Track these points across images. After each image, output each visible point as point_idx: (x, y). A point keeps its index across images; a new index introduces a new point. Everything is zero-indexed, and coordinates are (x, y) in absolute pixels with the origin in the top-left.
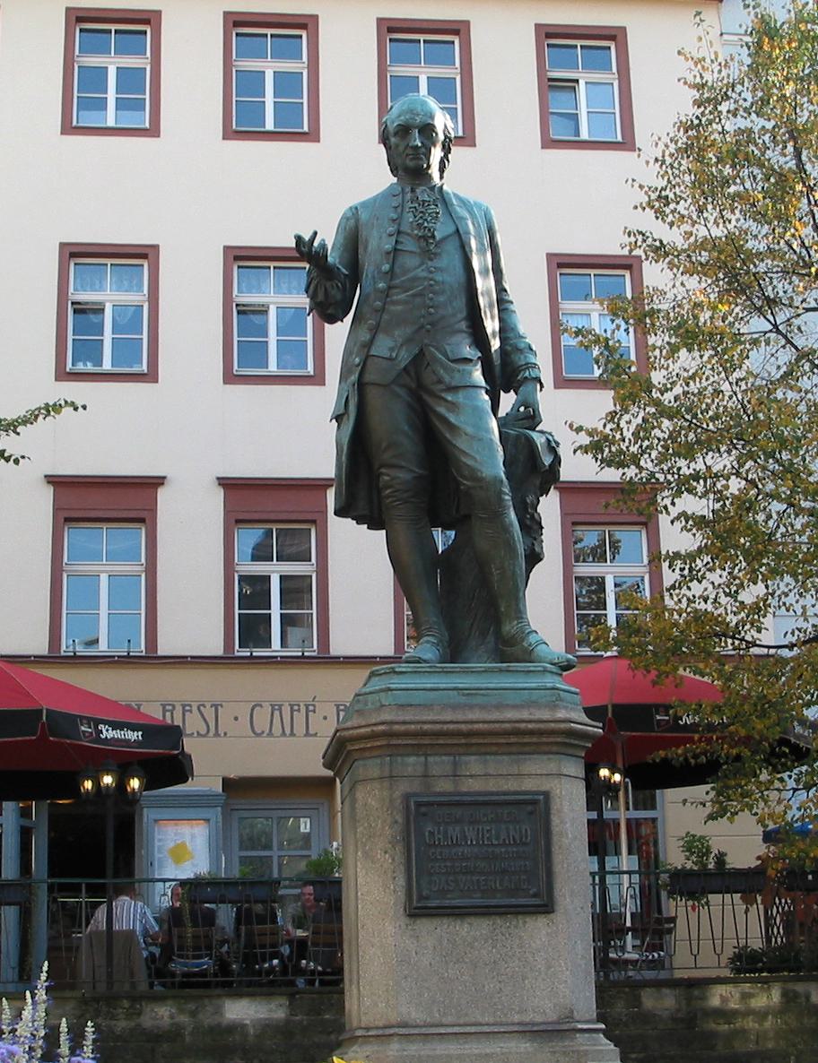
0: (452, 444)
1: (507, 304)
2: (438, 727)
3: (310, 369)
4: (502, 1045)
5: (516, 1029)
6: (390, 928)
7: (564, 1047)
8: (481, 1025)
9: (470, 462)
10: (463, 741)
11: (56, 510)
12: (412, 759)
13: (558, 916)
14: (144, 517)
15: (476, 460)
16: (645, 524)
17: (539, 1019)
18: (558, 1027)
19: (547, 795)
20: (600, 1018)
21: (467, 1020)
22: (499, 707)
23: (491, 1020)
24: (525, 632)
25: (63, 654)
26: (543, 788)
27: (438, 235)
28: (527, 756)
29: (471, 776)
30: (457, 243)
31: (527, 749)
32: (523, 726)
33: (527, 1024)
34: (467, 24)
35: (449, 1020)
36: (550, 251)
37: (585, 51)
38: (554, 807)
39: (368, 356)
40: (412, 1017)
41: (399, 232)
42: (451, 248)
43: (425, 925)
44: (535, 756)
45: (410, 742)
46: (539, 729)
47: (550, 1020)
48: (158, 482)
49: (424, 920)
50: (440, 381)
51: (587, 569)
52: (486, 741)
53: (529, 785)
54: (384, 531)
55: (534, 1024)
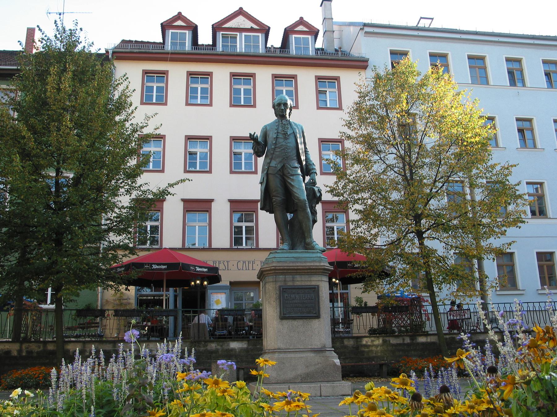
2: (288, 267)
3: (254, 170)
6: (275, 322)
9: (297, 195)
12: (281, 276)
13: (321, 319)
14: (208, 210)
17: (316, 347)
19: (318, 286)
20: (333, 347)
22: (305, 262)
23: (303, 348)
24: (312, 242)
27: (288, 133)
30: (294, 136)
31: (313, 273)
32: (312, 267)
35: (291, 347)
38: (320, 289)
43: (285, 322)
49: (285, 320)
50: (289, 173)
51: (329, 224)
53: (313, 283)
55: (315, 349)
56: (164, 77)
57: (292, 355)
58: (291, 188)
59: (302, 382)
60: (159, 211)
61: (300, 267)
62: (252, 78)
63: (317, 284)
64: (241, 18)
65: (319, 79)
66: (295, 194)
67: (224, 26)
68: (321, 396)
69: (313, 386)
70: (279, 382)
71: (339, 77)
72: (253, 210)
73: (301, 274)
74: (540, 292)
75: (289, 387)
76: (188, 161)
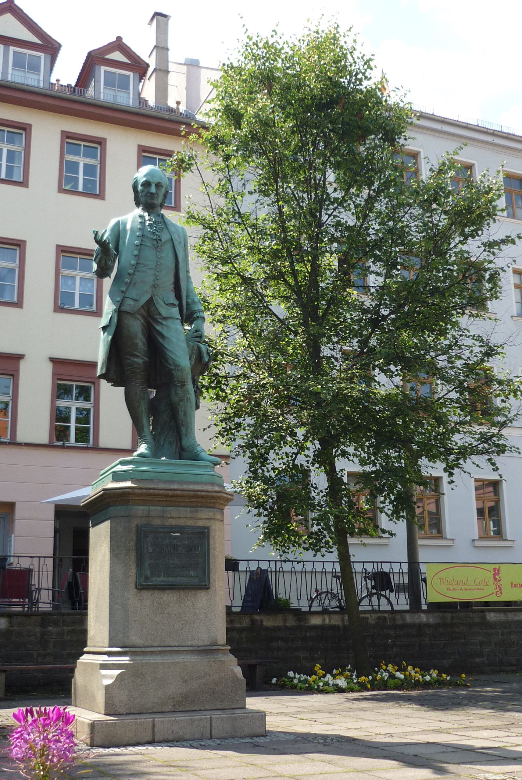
0: (164, 346)
2: (157, 491)
3: (94, 308)
4: (183, 657)
7: (214, 658)
8: (172, 646)
9: (173, 356)
10: (168, 499)
11: (54, 374)
12: (141, 507)
15: (176, 355)
16: (13, 375)
17: (201, 643)
18: (210, 648)
19: (208, 528)
21: (165, 644)
22: (187, 483)
23: (177, 644)
24: (195, 445)
27: (163, 240)
28: (200, 509)
29: (171, 518)
30: (171, 245)
32: (199, 493)
33: (195, 646)
34: (30, 126)
35: (155, 644)
36: (59, 244)
37: (85, 148)
38: (212, 534)
39: (124, 297)
40: (138, 642)
41: (143, 236)
42: (168, 247)
43: (146, 594)
44: (203, 509)
45: (142, 498)
47: (206, 644)
49: (145, 591)
50: (160, 314)
51: (62, 403)
52: (180, 500)
53: (200, 523)
54: (123, 389)
55: (199, 646)
57: (158, 659)
58: (160, 340)
59: (174, 712)
61: (178, 492)
62: (24, 132)
63: (206, 525)
64: (8, 17)
65: (68, 137)
66: (167, 352)
67: (108, 57)
68: (211, 738)
70: (132, 711)
71: (105, 140)
74: (477, 543)
75: (154, 720)
76: (16, 284)
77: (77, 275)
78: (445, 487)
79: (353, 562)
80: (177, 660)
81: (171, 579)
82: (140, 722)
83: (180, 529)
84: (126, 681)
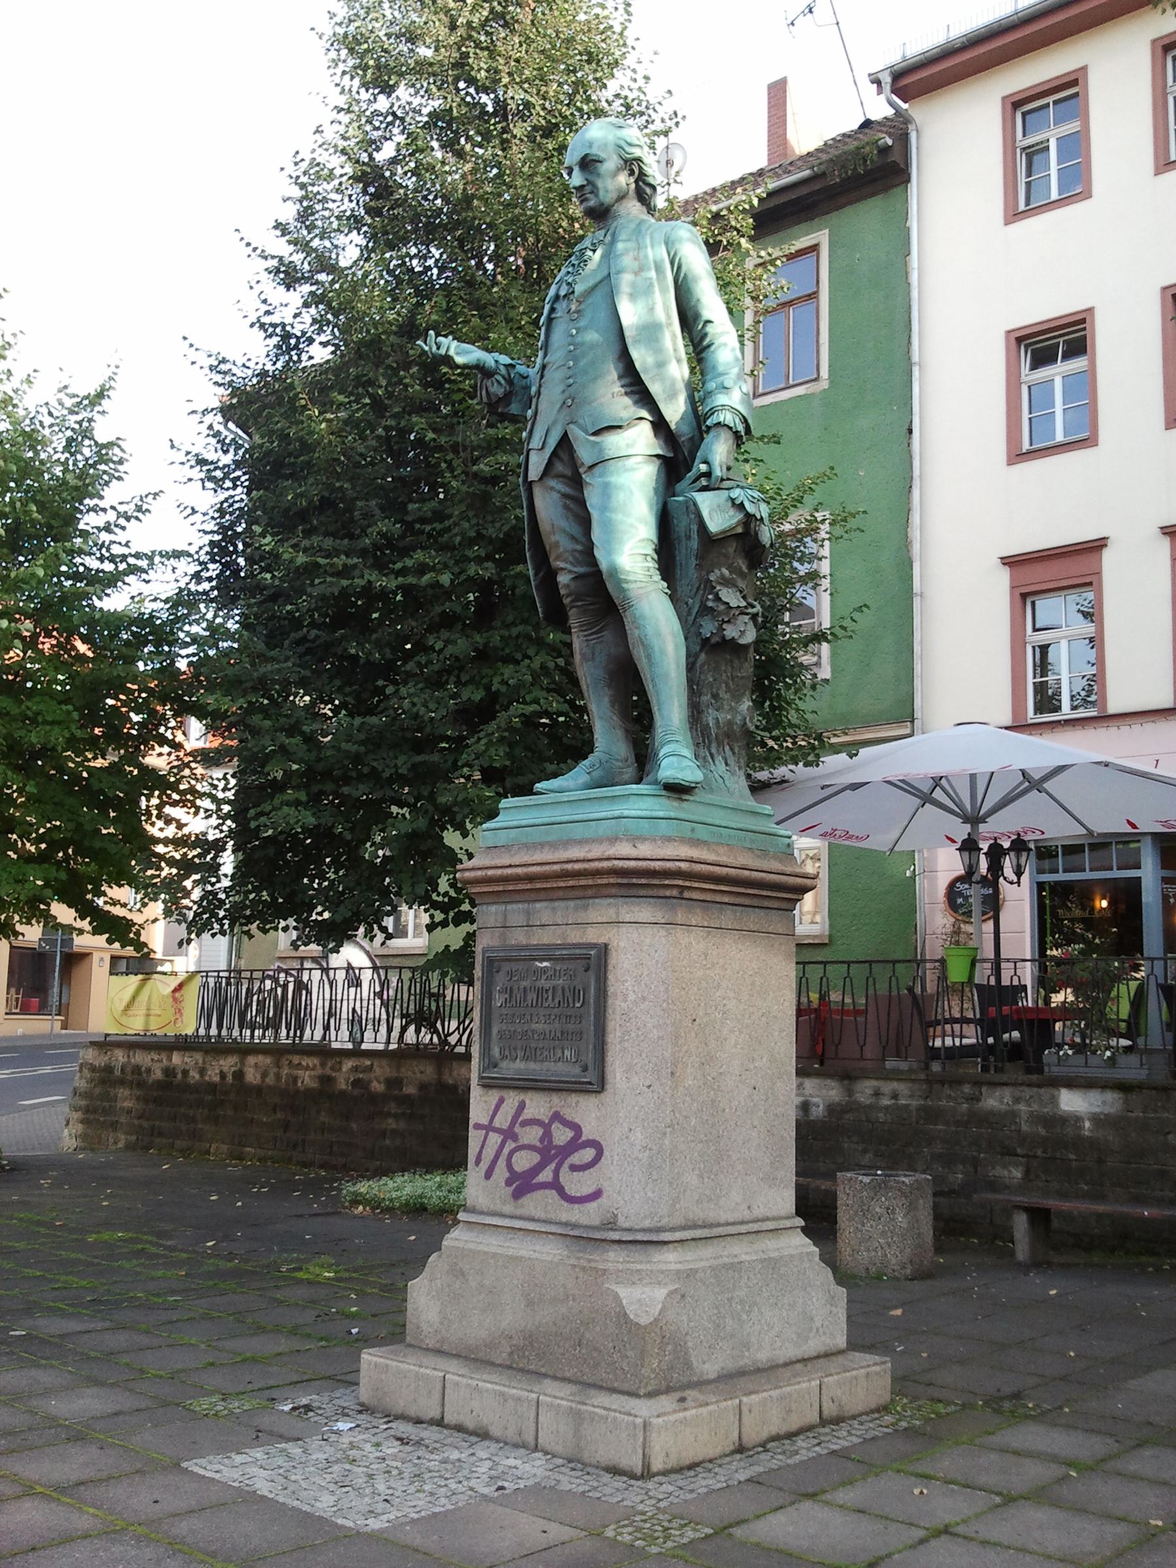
1: (722, 378)
5: (553, 1230)
12: (493, 908)
14: (1090, 582)
20: (799, 1212)
22: (568, 843)
23: (543, 1216)
25: (1030, 721)
26: (602, 940)
28: (591, 901)
31: (590, 892)
38: (612, 961)
44: (597, 900)
46: (527, 874)
48: (1097, 546)
56: (815, 248)
60: (1090, 584)
69: (513, 1397)
70: (445, 1348)
72: (1087, 580)
73: (552, 895)
77: (1054, 375)
78: (579, 774)
79: (335, 969)
80: (523, 1253)
81: (532, 1065)
82: (423, 1375)
83: (547, 952)
84: (439, 1282)
